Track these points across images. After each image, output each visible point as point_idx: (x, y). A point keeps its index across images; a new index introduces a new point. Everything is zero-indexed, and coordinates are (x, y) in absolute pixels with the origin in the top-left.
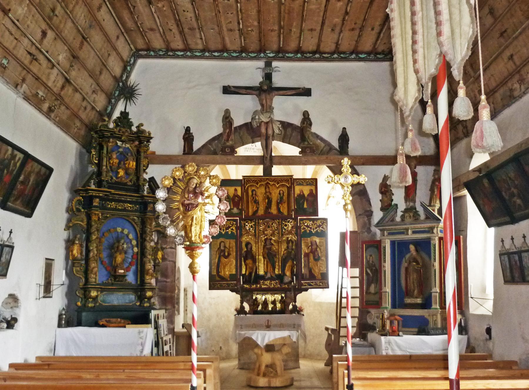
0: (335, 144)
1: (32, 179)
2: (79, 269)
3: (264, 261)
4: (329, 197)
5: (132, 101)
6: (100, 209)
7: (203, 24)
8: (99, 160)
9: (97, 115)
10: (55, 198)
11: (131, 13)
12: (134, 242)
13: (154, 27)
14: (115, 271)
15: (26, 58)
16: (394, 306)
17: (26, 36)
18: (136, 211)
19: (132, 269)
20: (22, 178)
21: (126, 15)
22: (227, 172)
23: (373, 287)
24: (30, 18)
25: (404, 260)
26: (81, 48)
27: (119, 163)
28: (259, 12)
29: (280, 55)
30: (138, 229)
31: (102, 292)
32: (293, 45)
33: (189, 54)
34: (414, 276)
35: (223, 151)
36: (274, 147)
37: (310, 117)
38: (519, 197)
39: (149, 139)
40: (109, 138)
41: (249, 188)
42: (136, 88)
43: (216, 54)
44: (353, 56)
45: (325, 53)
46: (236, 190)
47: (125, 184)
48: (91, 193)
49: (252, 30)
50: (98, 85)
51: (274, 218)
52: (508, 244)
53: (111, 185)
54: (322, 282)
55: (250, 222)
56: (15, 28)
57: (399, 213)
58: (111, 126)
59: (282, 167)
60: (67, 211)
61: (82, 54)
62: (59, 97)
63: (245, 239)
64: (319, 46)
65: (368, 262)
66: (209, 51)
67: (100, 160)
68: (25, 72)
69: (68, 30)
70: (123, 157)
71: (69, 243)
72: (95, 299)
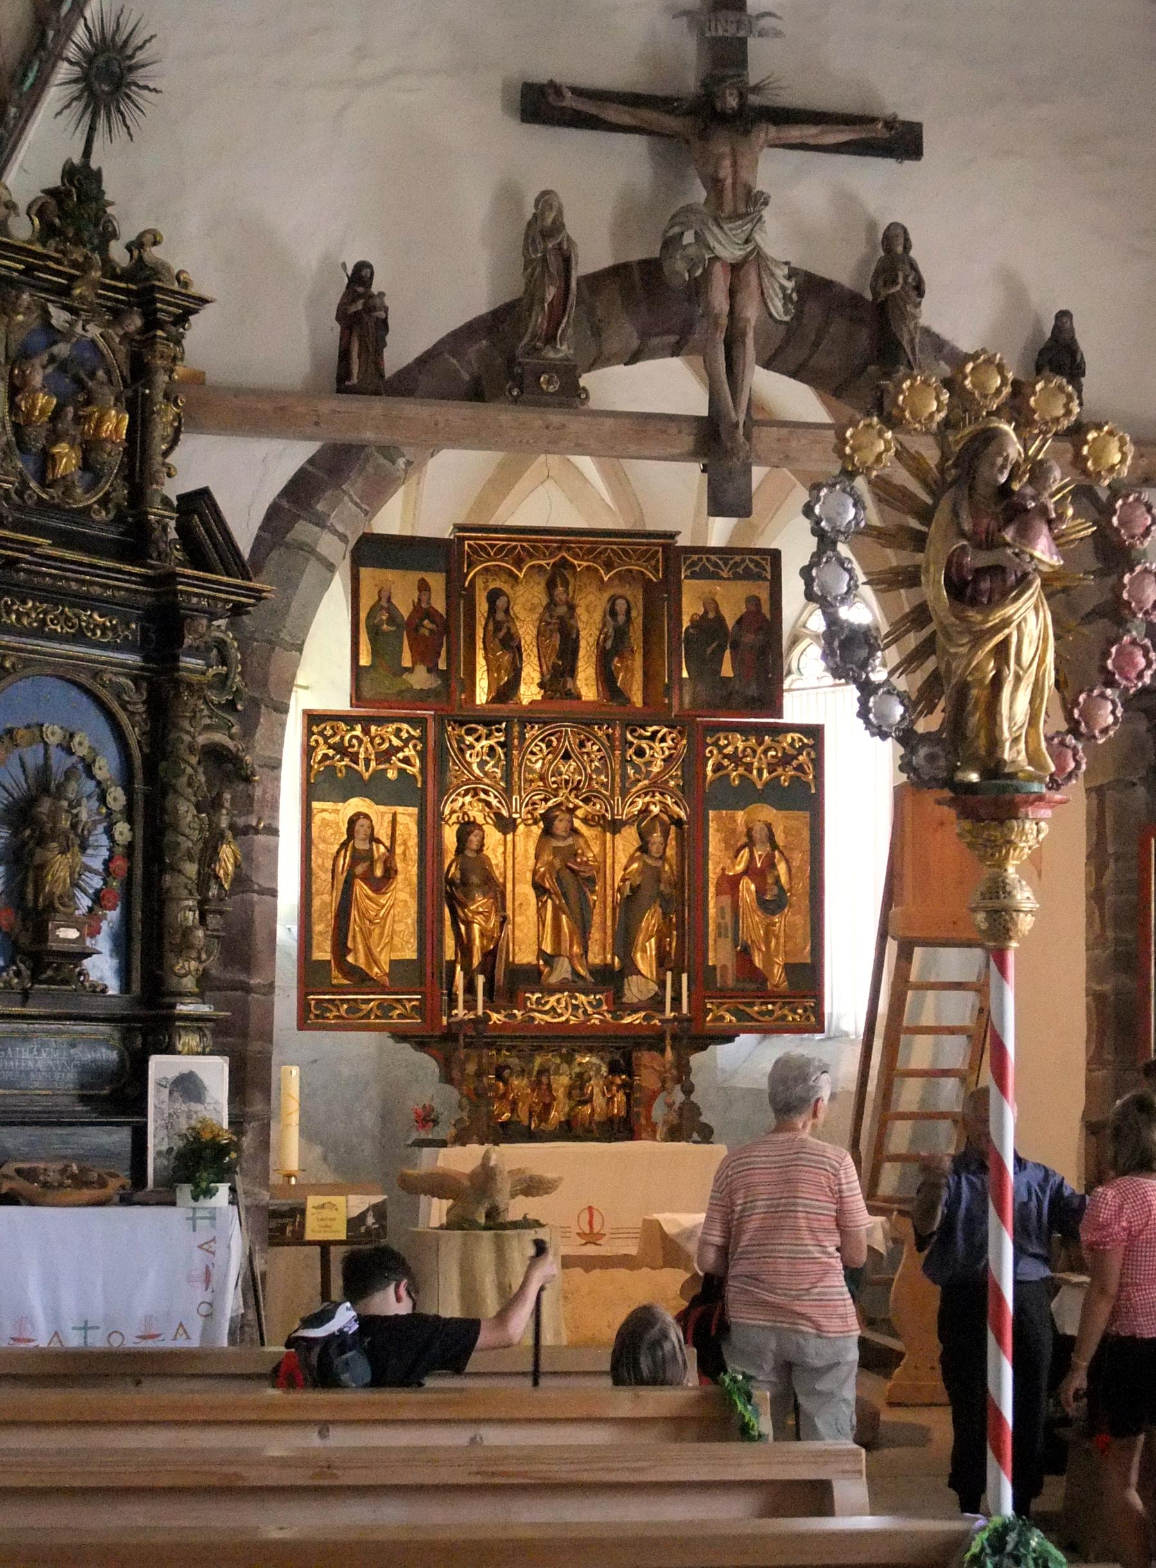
3: (541, 910)
5: (116, 118)
12: (117, 797)
19: (104, 925)
30: (133, 735)
41: (479, 583)
42: (140, 56)
46: (423, 587)
51: (586, 721)
55: (482, 730)
63: (460, 805)
70: (75, 381)
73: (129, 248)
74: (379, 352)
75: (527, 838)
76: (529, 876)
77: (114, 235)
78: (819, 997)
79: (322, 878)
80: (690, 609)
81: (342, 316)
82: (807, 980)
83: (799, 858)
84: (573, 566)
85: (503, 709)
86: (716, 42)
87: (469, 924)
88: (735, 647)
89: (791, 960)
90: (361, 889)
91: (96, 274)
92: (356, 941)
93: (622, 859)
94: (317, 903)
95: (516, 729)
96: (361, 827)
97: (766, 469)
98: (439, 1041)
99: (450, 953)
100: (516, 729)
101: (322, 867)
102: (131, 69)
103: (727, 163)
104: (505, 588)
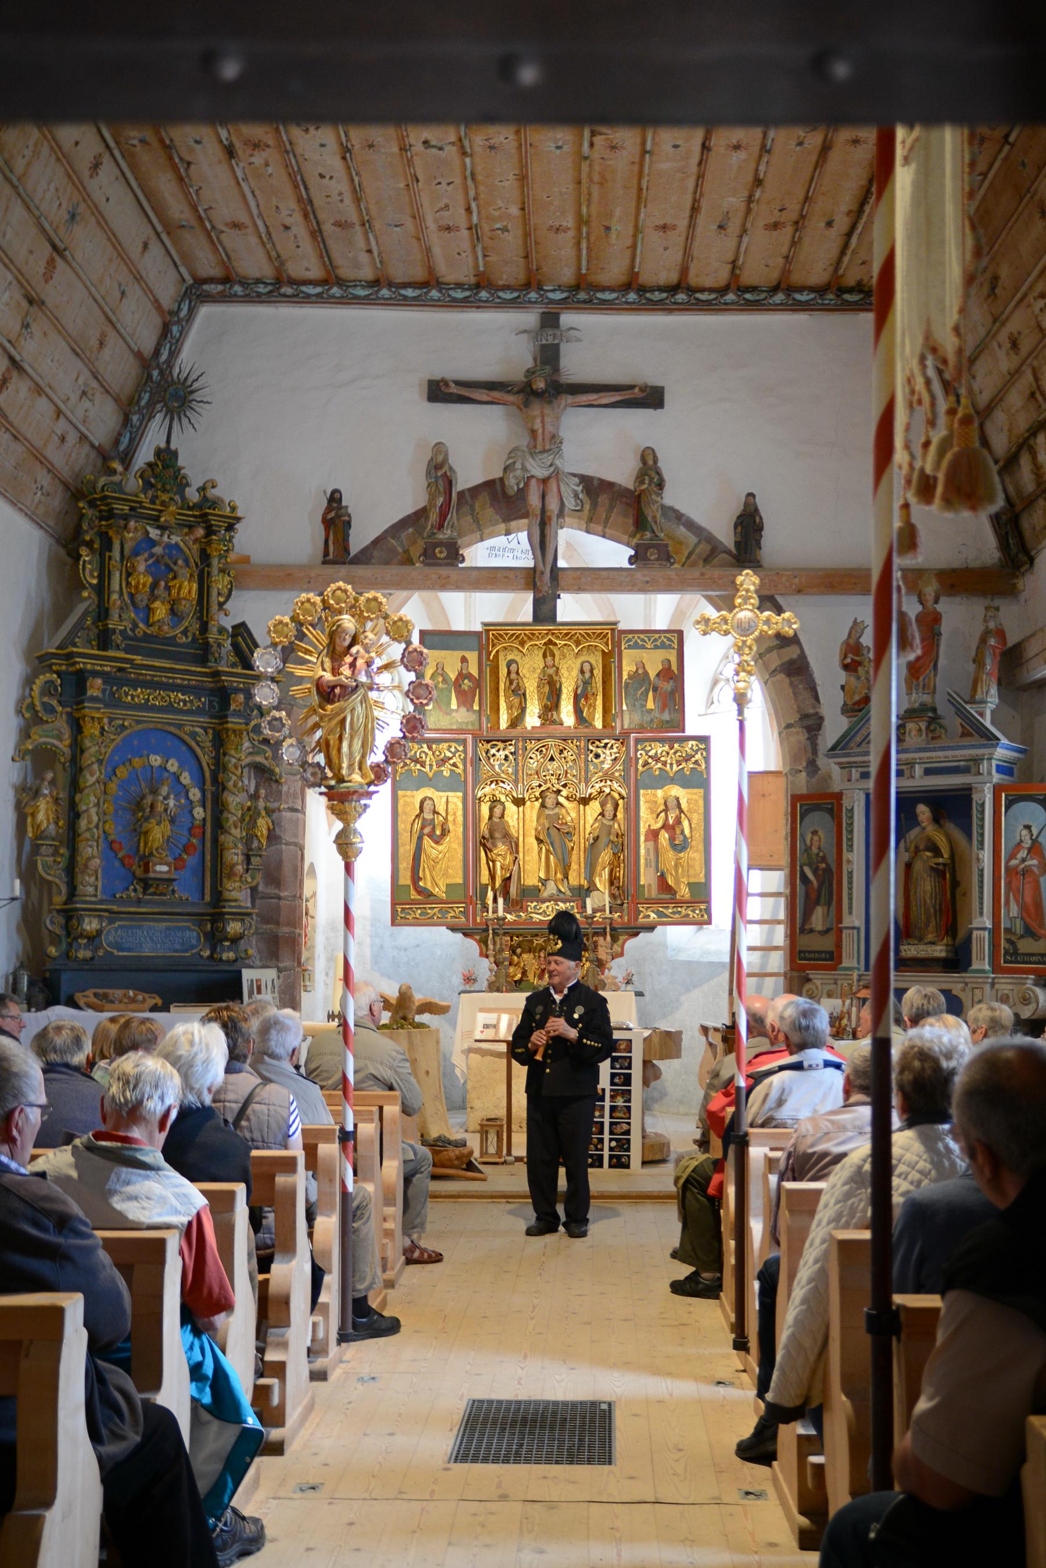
0: (725, 535)
4: (715, 682)
6: (107, 706)
7: (374, 212)
8: (101, 577)
9: (93, 455)
11: (181, 179)
12: (195, 794)
13: (243, 218)
14: (147, 870)
21: (165, 184)
23: (819, 912)
26: (48, 277)
27: (154, 586)
28: (523, 178)
29: (582, 296)
30: (205, 760)
31: (111, 921)
32: (614, 271)
33: (335, 291)
35: (429, 556)
36: (569, 545)
37: (660, 464)
40: (126, 518)
42: (196, 385)
43: (410, 292)
44: (780, 297)
45: (702, 290)
46: (464, 660)
47: (172, 641)
48: (82, 663)
49: (505, 229)
54: (696, 905)
55: (501, 745)
58: (133, 484)
59: (587, 597)
60: (19, 712)
61: (51, 293)
64: (684, 271)
65: (807, 849)
66: (390, 285)
67: (104, 575)
70: (164, 570)
72: (93, 938)
73: (198, 490)
75: (532, 809)
76: (533, 832)
77: (188, 485)
78: (708, 902)
79: (404, 836)
80: (628, 668)
81: (325, 521)
82: (701, 894)
83: (697, 818)
84: (555, 644)
85: (514, 732)
86: (543, 346)
87: (494, 862)
88: (655, 689)
89: (692, 880)
90: (427, 841)
91: (173, 508)
92: (425, 872)
93: (590, 820)
94: (401, 850)
95: (520, 744)
96: (428, 804)
97: (519, 619)
98: (478, 932)
99: (485, 878)
100: (520, 744)
101: (405, 830)
102: (192, 392)
103: (538, 420)
104: (518, 659)
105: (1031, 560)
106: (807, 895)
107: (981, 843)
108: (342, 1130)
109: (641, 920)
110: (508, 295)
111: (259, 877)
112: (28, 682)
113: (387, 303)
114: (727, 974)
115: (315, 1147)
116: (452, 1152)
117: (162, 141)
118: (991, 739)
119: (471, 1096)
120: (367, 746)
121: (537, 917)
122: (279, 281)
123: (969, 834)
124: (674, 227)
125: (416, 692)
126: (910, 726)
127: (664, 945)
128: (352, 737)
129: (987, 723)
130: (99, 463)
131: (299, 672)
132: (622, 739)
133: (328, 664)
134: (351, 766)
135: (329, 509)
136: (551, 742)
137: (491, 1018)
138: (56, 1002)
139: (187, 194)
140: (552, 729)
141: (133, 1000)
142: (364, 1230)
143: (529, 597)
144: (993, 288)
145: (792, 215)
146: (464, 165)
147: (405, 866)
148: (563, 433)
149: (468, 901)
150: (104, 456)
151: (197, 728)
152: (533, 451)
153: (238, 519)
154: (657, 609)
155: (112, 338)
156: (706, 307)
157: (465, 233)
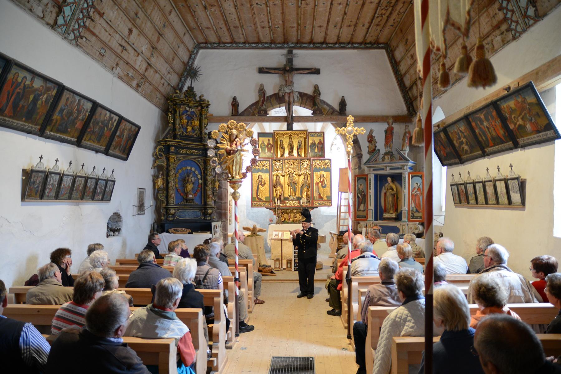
0: (336, 107)
1: (126, 133)
2: (162, 196)
4: (332, 145)
6: (176, 154)
7: (244, 23)
8: (174, 121)
9: (172, 89)
10: (144, 148)
11: (193, 16)
12: (199, 176)
13: (210, 26)
14: (187, 196)
15: (118, 49)
16: (376, 219)
17: (117, 32)
18: (199, 155)
20: (118, 133)
21: (189, 18)
22: (262, 128)
23: (362, 206)
24: (120, 19)
25: (383, 188)
26: (158, 41)
27: (188, 122)
28: (283, 13)
29: (299, 45)
30: (201, 167)
31: (178, 210)
32: (307, 38)
33: (234, 45)
34: (390, 199)
35: (259, 114)
36: (295, 111)
38: (467, 144)
39: (208, 106)
40: (180, 105)
43: (253, 45)
44: (350, 45)
45: (330, 44)
46: (269, 140)
47: (192, 137)
48: (169, 143)
49: (278, 27)
50: (172, 68)
52: (457, 179)
53: (184, 138)
54: (328, 201)
56: (109, 26)
57: (381, 156)
58: (183, 96)
59: (300, 124)
60: (153, 156)
61: (159, 46)
62: (144, 77)
64: (325, 38)
65: (359, 189)
66: (248, 43)
67: (175, 120)
68: (118, 59)
69: (148, 28)
70: (190, 118)
71: (155, 178)
72: (173, 215)
74: (238, 109)
75: (287, 177)
78: (331, 201)
79: (254, 185)
80: (310, 141)
81: (232, 105)
82: (329, 199)
83: (328, 179)
90: (260, 186)
92: (260, 194)
93: (301, 180)
96: (260, 177)
97: (283, 129)
98: (274, 209)
99: (275, 195)
105: (416, 113)
106: (359, 201)
107: (405, 188)
108: (235, 278)
109: (314, 205)
110: (279, 45)
111: (216, 198)
112: (155, 148)
113: (248, 48)
114: (336, 219)
115: (227, 283)
116: (267, 269)
117: (187, 5)
118: (407, 160)
119: (272, 250)
120: (240, 168)
121: (288, 205)
122: (220, 42)
123: (402, 186)
124: (323, 26)
125: (255, 151)
126: (386, 157)
127: (320, 211)
128: (236, 165)
129: (406, 156)
130: (174, 91)
131: (221, 146)
132: (309, 159)
133: (229, 144)
134: (236, 174)
135: (233, 101)
136: (291, 161)
137: (277, 233)
138: (164, 232)
139: (195, 20)
140: (291, 157)
141: (184, 231)
142: (242, 303)
143: (286, 124)
144: (406, 42)
145: (354, 23)
146: (267, 10)
147: (255, 192)
148: (294, 81)
149: (271, 201)
150: (174, 89)
151: (199, 159)
152: (286, 85)
153: (209, 105)
154: (317, 127)
155: (176, 58)
156: (331, 48)
157: (268, 29)
